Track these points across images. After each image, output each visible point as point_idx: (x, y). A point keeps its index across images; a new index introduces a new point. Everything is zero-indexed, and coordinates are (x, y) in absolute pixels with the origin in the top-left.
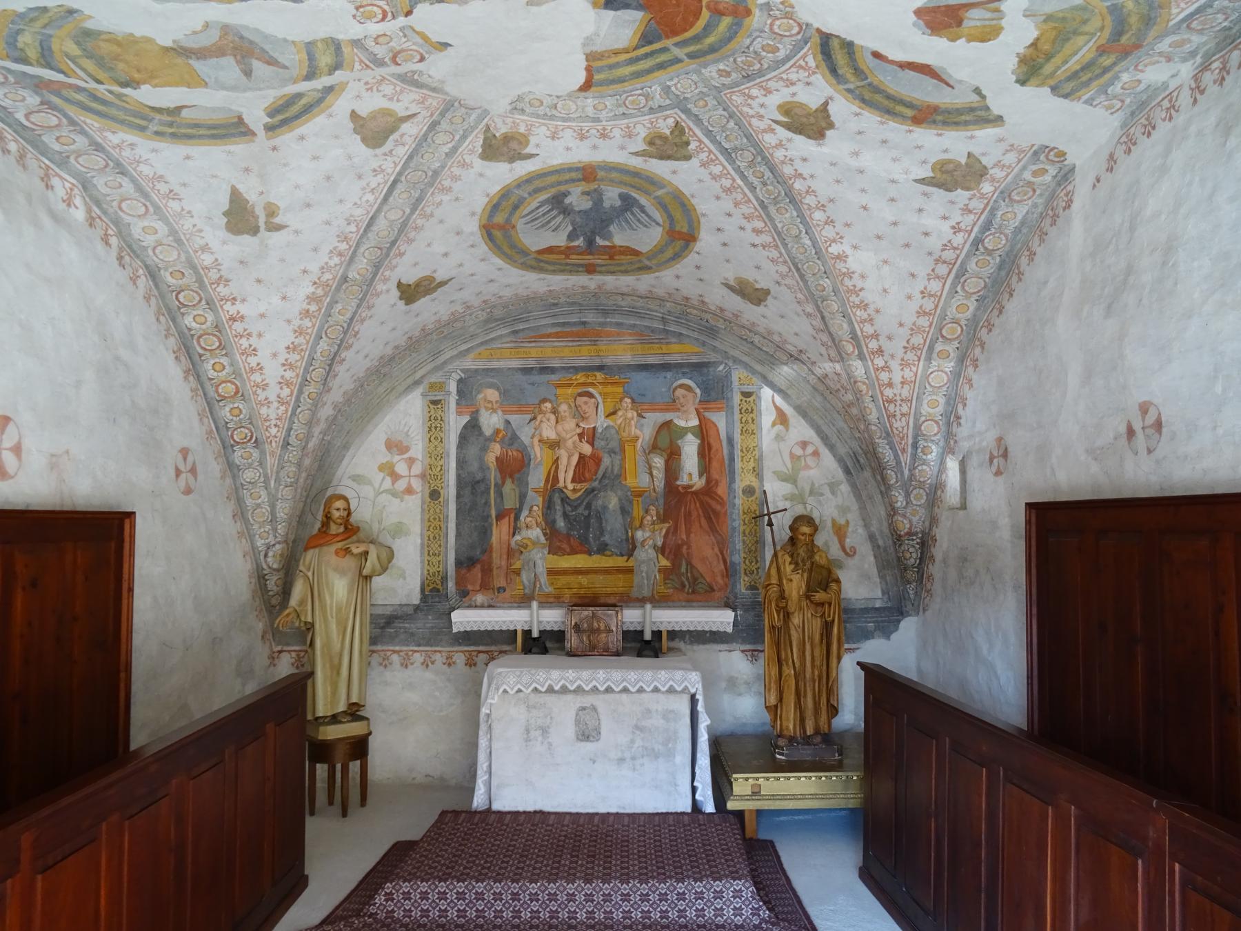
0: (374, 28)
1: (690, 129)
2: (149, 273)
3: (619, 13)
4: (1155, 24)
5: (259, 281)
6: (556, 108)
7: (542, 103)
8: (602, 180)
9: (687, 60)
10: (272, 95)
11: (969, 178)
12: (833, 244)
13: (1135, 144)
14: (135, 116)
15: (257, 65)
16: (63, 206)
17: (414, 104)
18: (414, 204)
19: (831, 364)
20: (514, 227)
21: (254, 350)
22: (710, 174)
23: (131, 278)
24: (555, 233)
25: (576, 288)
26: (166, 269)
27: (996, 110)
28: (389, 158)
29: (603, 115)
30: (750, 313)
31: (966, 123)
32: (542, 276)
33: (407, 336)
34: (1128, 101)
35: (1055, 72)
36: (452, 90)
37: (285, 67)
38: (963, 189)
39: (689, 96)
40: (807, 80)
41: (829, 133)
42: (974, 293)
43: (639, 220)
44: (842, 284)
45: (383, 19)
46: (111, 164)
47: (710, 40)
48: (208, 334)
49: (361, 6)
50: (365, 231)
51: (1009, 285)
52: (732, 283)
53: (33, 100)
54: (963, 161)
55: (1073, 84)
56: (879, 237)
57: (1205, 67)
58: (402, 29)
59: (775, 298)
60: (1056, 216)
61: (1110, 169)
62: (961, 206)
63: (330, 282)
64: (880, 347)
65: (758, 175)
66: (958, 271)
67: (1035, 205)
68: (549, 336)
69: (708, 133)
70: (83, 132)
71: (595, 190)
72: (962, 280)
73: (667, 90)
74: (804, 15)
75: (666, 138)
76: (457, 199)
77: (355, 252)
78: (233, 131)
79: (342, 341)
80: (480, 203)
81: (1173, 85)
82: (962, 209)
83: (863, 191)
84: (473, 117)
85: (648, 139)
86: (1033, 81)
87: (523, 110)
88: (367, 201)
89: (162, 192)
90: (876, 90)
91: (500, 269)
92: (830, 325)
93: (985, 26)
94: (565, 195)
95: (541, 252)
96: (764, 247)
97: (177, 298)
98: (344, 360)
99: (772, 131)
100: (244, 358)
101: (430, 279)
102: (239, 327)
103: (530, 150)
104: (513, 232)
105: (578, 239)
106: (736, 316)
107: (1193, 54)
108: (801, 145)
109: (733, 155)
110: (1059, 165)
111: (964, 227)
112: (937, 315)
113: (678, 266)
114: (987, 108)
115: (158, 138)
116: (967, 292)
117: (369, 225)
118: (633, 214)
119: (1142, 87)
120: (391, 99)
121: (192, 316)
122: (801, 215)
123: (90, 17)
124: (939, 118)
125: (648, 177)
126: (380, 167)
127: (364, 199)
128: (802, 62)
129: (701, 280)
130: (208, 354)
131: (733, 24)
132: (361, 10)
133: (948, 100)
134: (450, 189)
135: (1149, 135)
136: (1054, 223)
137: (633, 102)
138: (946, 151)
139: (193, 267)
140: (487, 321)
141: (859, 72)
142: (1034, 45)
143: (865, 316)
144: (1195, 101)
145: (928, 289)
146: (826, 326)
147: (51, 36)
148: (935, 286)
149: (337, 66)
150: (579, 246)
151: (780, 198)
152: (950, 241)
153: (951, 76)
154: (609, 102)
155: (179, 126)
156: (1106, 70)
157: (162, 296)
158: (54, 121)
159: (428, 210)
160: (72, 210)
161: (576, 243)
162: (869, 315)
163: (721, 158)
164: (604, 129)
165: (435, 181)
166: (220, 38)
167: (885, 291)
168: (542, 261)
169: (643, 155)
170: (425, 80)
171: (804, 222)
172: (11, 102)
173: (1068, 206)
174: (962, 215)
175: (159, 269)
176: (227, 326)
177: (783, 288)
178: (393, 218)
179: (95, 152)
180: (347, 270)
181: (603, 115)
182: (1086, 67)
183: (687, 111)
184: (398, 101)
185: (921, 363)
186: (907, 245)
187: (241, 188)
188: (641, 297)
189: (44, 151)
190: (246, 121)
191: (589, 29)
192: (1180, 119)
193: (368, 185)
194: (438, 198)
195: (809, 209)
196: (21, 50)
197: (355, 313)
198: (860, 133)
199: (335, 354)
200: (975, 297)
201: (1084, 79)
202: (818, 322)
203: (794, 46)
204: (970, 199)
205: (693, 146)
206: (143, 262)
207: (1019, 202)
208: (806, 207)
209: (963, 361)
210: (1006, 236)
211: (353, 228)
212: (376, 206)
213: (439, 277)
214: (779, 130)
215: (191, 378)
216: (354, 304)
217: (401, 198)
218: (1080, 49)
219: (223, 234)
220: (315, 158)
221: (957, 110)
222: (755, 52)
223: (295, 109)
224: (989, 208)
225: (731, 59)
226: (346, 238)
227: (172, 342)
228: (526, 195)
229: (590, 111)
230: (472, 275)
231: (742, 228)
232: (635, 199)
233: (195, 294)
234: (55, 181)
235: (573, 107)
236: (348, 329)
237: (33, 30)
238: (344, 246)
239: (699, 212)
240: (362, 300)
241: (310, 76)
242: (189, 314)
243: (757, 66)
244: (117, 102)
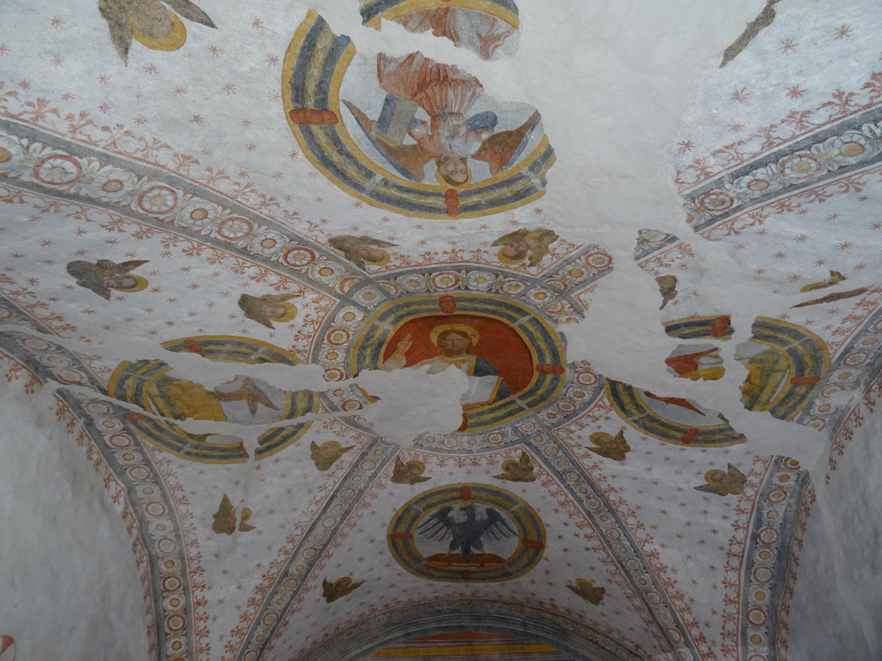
0: (334, 384)
1: (533, 458)
2: (151, 561)
3: (483, 378)
4: (822, 362)
5: (225, 572)
6: (443, 443)
7: (434, 439)
8: (474, 498)
9: (527, 408)
10: (263, 429)
11: (734, 485)
12: (646, 544)
13: (843, 447)
14: (177, 440)
15: (260, 406)
16: (111, 501)
17: (352, 439)
18: (343, 515)
19: (664, 655)
20: (411, 536)
21: (208, 632)
22: (550, 492)
23: (137, 561)
24: (440, 542)
25: (456, 595)
26: (163, 559)
27: (738, 430)
28: (331, 478)
29: (474, 448)
30: (592, 612)
31: (720, 441)
32: (430, 581)
33: (324, 632)
34: (827, 420)
35: (768, 400)
36: (378, 430)
37: (277, 409)
38: (731, 493)
39: (530, 433)
40: (606, 415)
41: (627, 454)
42: (765, 582)
43: (501, 531)
44: (659, 578)
45: (340, 379)
46: (151, 475)
47: (541, 391)
48: (177, 616)
49: (329, 370)
50: (307, 535)
51: (791, 571)
52: (574, 584)
53: (119, 426)
54: (726, 471)
55: (784, 408)
56: (679, 536)
57: (868, 390)
58: (351, 386)
59: (609, 596)
60: (807, 509)
61: (834, 468)
62: (735, 507)
63: (275, 576)
64: (701, 634)
65: (583, 491)
66: (747, 563)
67: (790, 505)
68: (434, 637)
69: (545, 461)
70: (141, 451)
71: (470, 506)
72: (753, 571)
73: (515, 430)
74: (597, 370)
75: (517, 464)
76: (373, 513)
77: (297, 551)
78: (235, 454)
79: (274, 628)
80: (388, 515)
81: (853, 405)
82: (737, 510)
83: (660, 498)
84: (389, 450)
85: (505, 466)
86: (756, 407)
87: (422, 445)
88: (312, 511)
89: (178, 498)
90: (653, 419)
91: (399, 575)
92: (656, 616)
93: (712, 369)
94: (449, 509)
95: (431, 559)
96: (595, 550)
97: (163, 584)
98: (273, 647)
99: (588, 456)
100: (198, 638)
101: (347, 580)
102: (201, 610)
103: (425, 474)
104: (410, 541)
105: (458, 548)
106: (581, 616)
107: (857, 384)
108: (610, 465)
109: (564, 476)
110: (796, 471)
111: (741, 525)
112: (741, 603)
113: (532, 571)
114: (732, 429)
115: (187, 457)
116: (760, 581)
117: (310, 530)
118: (497, 526)
119: (832, 410)
120: (338, 435)
121: (170, 599)
122: (618, 521)
123: (172, 369)
124: (700, 438)
125: (506, 495)
126: (324, 484)
127: (310, 509)
128: (600, 403)
129: (551, 584)
130: (172, 633)
131: (554, 379)
132: (328, 372)
133: (702, 424)
134: (369, 505)
135: (850, 438)
136: (808, 515)
137: (493, 439)
138: (711, 463)
139: (182, 558)
140: (387, 625)
141: (639, 408)
142: (748, 380)
143: (683, 606)
144: (871, 410)
145: (728, 580)
146: (653, 616)
147: (145, 381)
148: (732, 577)
149: (308, 410)
150: (457, 554)
151: (601, 508)
152: (734, 537)
153: (700, 406)
154: (478, 439)
155: (202, 449)
156: (803, 397)
157: (154, 581)
158: (127, 442)
159: (353, 521)
160: (116, 504)
161: (456, 552)
162: (686, 605)
163: (556, 479)
164: (475, 459)
165: (359, 498)
166: (243, 386)
167: (694, 582)
168: (431, 567)
169: (502, 478)
170: (361, 422)
171: (622, 527)
172: (105, 428)
173: (813, 500)
174: (738, 514)
175: (158, 558)
176: (192, 609)
177: (614, 585)
178: (327, 525)
179: (144, 466)
180: (289, 566)
181: (474, 448)
182: (790, 395)
183: (529, 445)
184: (343, 436)
185: (740, 648)
186: (702, 542)
187: (230, 497)
188: (506, 603)
189: (111, 462)
190: (245, 446)
191: (465, 389)
192: (867, 423)
193: (314, 498)
194: (360, 512)
195: (624, 516)
196: (125, 390)
197: (288, 604)
198: (649, 453)
199: (268, 639)
200: (767, 586)
201: (790, 404)
202: (646, 615)
203: (594, 391)
204: (740, 501)
205: (535, 470)
206: (149, 552)
207: (777, 502)
208: (621, 514)
209: (774, 645)
210: (776, 531)
211: (299, 532)
212: (317, 515)
213: (355, 578)
214: (594, 455)
215: (154, 653)
216: (289, 596)
217: (335, 510)
218: (780, 383)
219: (209, 532)
220: (283, 476)
221: (711, 431)
222: (570, 398)
223: (277, 439)
224: (755, 508)
225: (555, 405)
226: (292, 539)
227: (150, 618)
228: (421, 510)
229: (466, 445)
230: (379, 579)
231: (577, 535)
232: (497, 513)
233: (177, 581)
234: (112, 484)
235: (455, 442)
236: (281, 619)
237: (136, 376)
238: (290, 546)
240: (295, 593)
241: (290, 416)
242: (168, 597)
243: (572, 408)
244: (169, 429)
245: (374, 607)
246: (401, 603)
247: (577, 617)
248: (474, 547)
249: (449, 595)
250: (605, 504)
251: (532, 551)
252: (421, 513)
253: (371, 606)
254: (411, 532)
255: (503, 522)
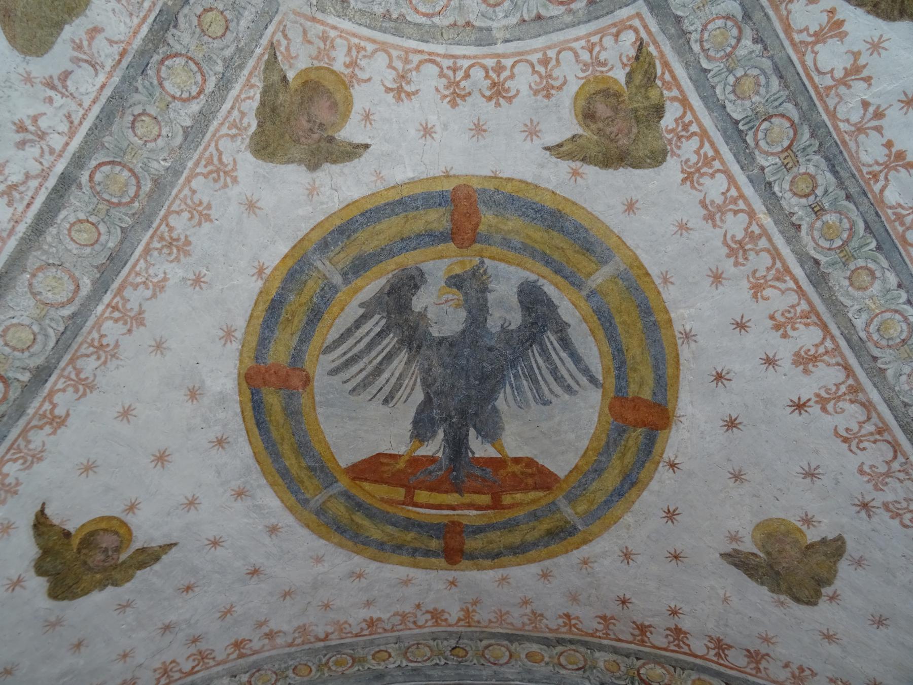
1: (666, 65)
8: (487, 240)
20: (307, 381)
22: (703, 204)
24: (386, 410)
43: (554, 372)
52: (748, 546)
69: (700, 77)
75: (617, 95)
76: (198, 281)
91: (273, 530)
96: (822, 402)
105: (434, 434)
106: (755, 657)
109: (750, 139)
113: (628, 518)
118: (544, 352)
125: (578, 227)
126: (35, 119)
150: (432, 460)
151: (854, 244)
163: (724, 150)
165: (154, 214)
168: (359, 506)
188: (546, 642)
228: (337, 279)
230: (215, 543)
231: (770, 362)
239: (677, 327)
245: (203, 646)
246: (279, 641)
247: (742, 661)
248: (479, 432)
249: (404, 616)
250: (868, 227)
251: (636, 436)
252: (335, 289)
253: (195, 641)
254: (307, 365)
255: (562, 329)
